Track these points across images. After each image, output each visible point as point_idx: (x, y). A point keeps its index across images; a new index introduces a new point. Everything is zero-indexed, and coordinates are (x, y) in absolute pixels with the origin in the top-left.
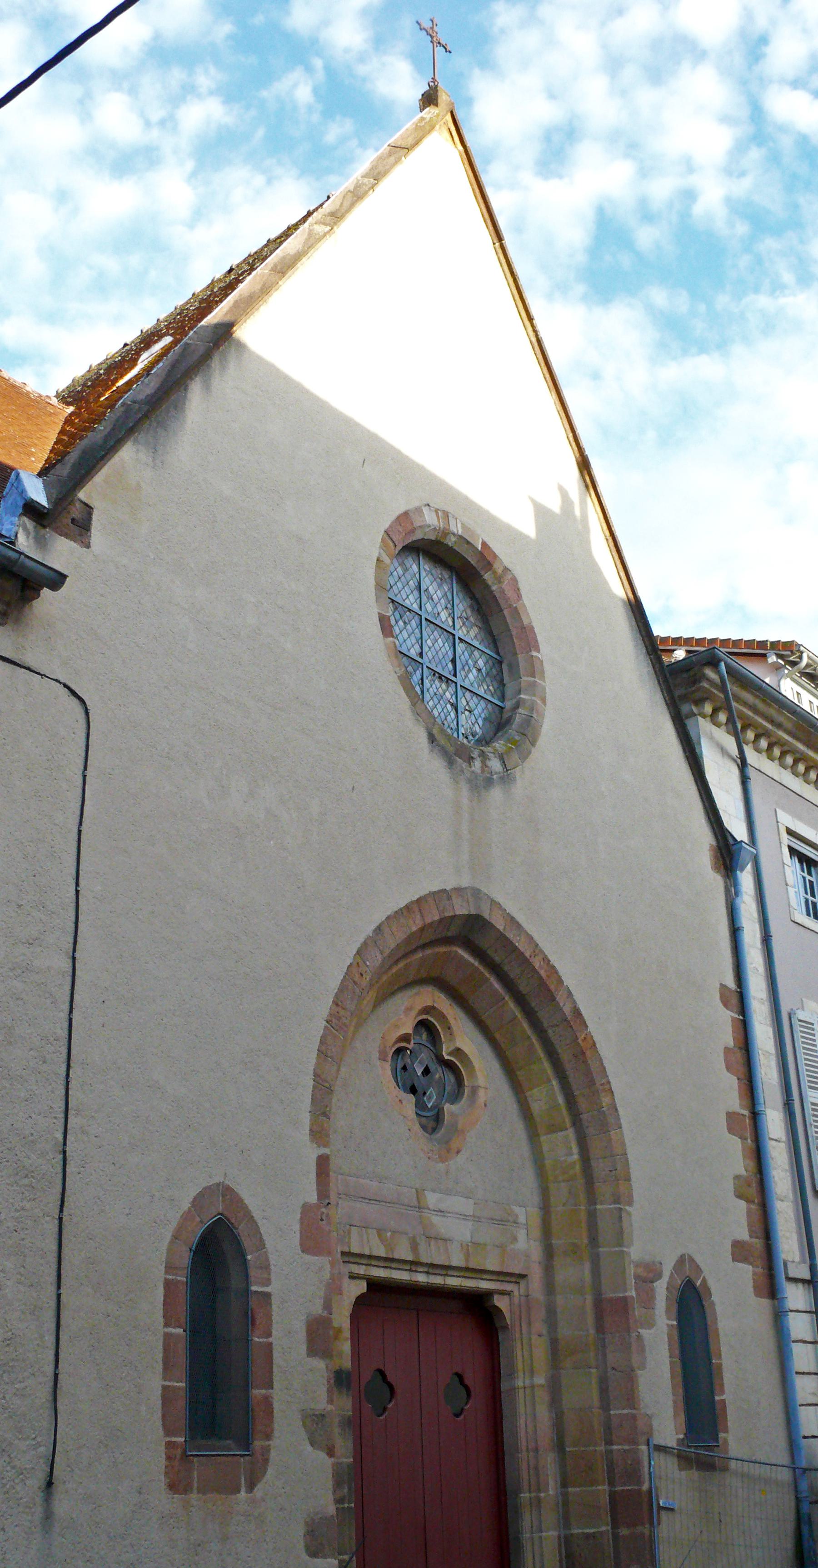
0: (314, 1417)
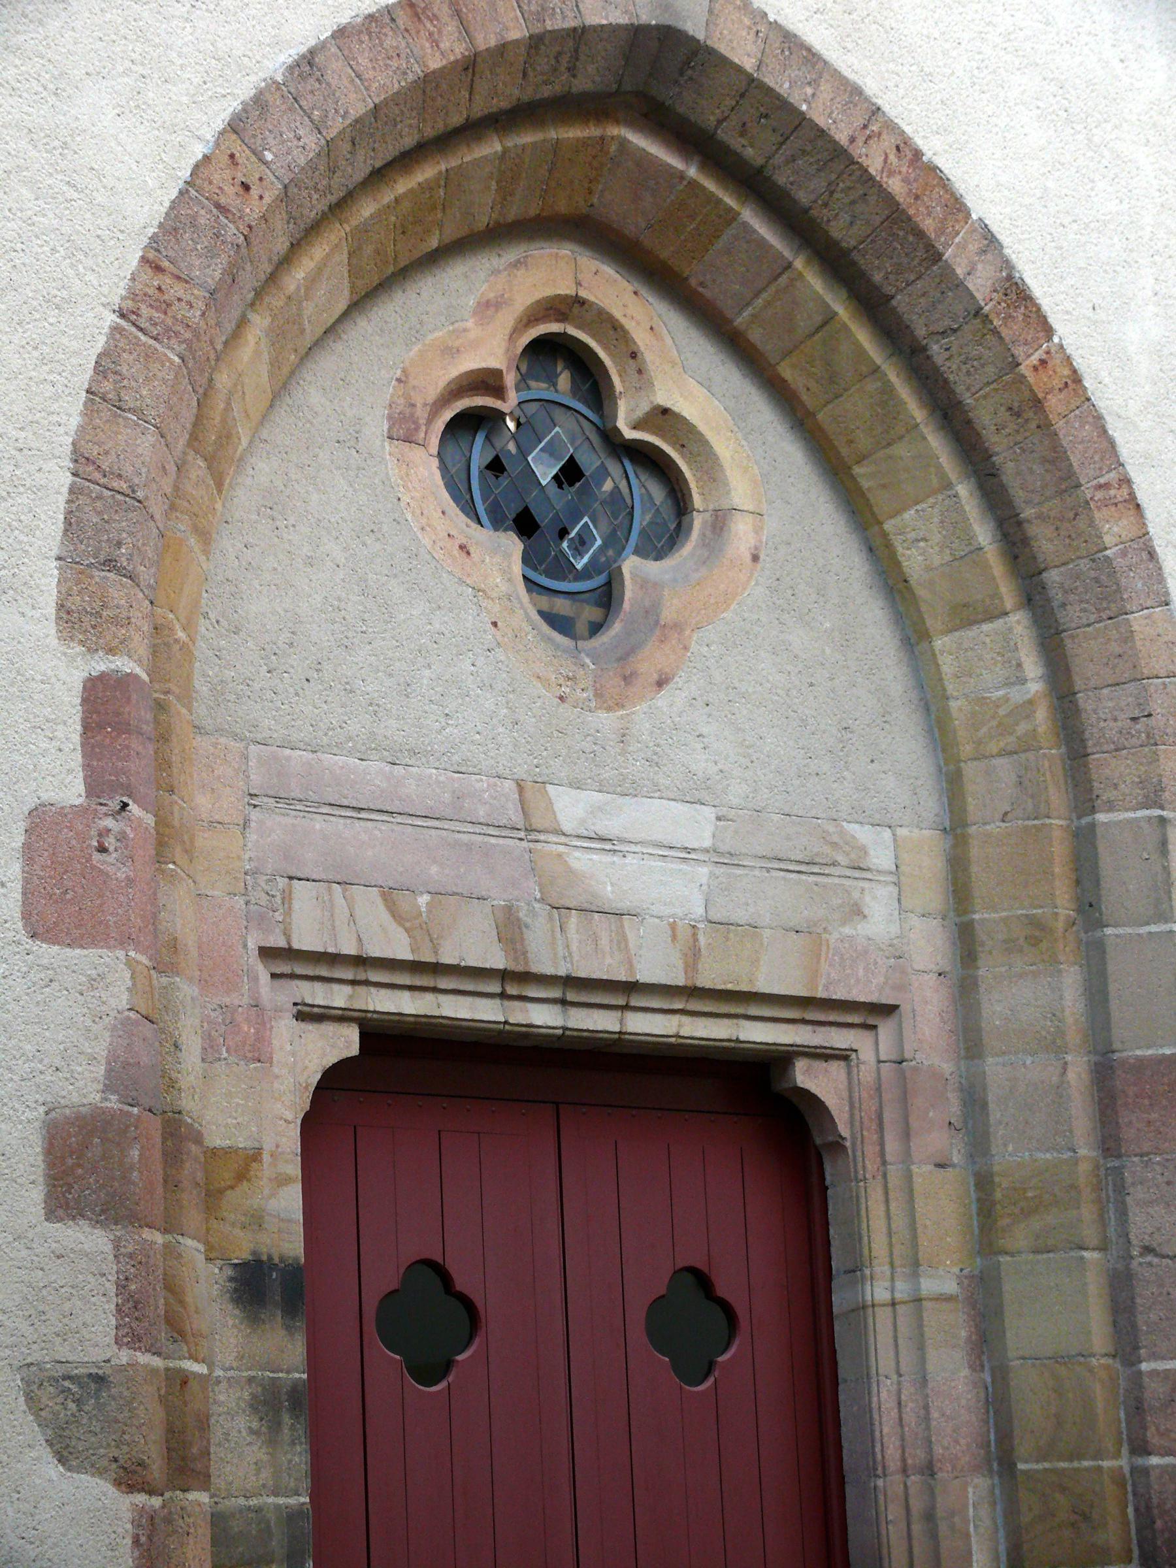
0: (67, 1384)
